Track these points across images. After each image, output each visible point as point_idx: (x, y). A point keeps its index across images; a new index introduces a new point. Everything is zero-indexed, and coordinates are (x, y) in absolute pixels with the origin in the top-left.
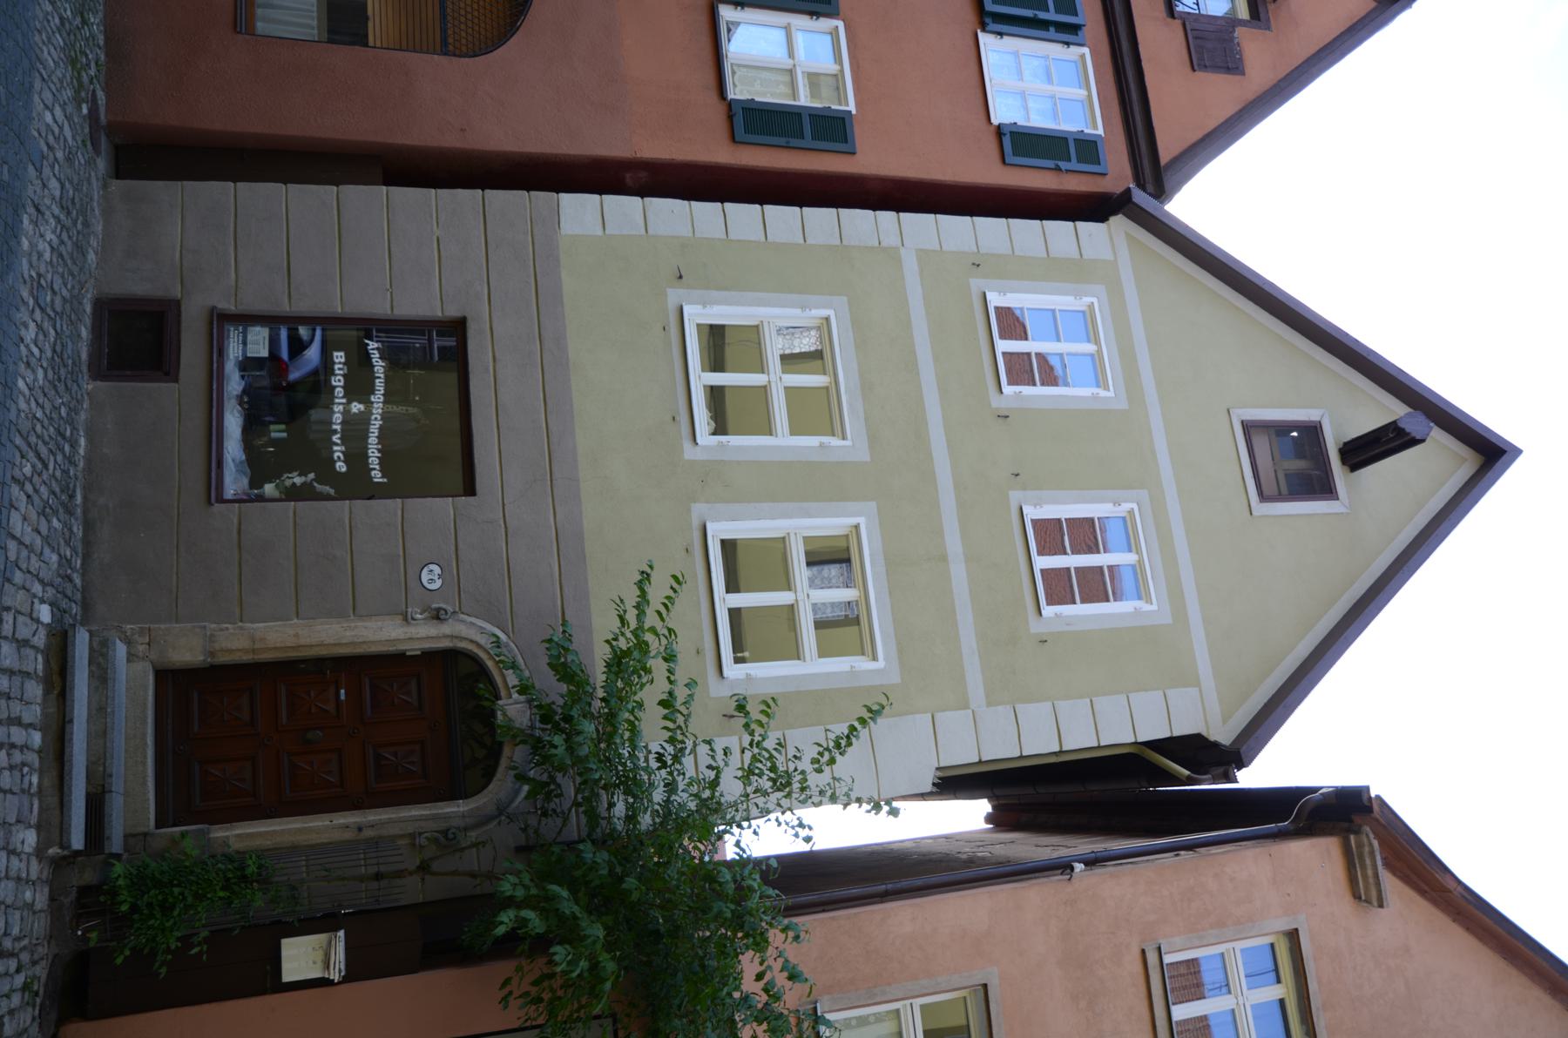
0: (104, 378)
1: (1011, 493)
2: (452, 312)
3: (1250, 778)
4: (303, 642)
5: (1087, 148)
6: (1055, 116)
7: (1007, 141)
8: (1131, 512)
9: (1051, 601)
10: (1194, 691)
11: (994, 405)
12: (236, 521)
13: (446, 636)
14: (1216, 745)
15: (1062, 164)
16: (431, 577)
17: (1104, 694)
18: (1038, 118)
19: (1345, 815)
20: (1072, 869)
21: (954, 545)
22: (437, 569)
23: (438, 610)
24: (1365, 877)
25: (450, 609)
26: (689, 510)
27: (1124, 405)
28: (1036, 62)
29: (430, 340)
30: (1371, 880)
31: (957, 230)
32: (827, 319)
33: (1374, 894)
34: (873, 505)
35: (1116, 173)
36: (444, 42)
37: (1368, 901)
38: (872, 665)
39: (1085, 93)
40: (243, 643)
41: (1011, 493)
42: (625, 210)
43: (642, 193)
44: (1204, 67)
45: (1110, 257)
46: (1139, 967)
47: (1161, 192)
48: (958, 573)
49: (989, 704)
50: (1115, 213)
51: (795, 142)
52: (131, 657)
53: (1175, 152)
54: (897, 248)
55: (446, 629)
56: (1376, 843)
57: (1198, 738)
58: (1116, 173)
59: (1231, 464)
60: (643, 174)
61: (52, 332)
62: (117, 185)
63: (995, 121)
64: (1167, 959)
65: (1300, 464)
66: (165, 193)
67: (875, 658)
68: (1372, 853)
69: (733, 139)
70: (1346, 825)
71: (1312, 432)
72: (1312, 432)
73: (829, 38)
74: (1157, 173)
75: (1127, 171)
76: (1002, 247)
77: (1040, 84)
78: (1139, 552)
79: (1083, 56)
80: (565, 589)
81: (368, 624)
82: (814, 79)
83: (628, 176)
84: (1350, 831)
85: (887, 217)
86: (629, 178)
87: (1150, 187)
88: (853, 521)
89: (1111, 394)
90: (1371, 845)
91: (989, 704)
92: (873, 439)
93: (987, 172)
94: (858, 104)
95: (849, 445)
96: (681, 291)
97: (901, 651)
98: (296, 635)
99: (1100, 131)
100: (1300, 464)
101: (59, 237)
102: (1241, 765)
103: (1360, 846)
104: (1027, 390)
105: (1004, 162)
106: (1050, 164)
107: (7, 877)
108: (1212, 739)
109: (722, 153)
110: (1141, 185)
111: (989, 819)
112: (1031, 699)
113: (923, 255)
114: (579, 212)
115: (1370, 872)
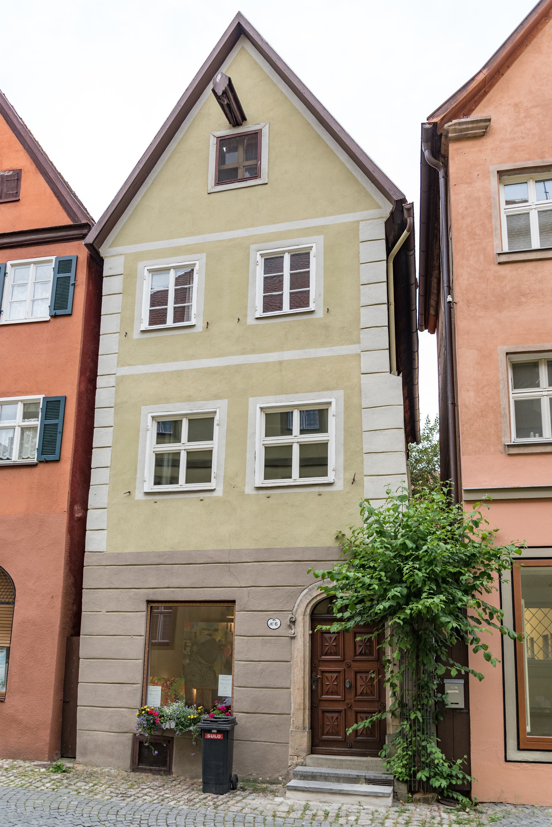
0: (170, 768)
1: (248, 324)
2: (143, 606)
3: (413, 193)
4: (302, 686)
5: (64, 266)
6: (46, 282)
7: (59, 312)
8: (262, 255)
9: (307, 305)
10: (362, 224)
11: (200, 329)
12: (242, 714)
13: (304, 619)
14: (392, 214)
15: (72, 282)
16: (275, 624)
17: (359, 278)
18: (46, 293)
19: (436, 141)
20: (450, 302)
21: (273, 357)
22: (271, 621)
23: (291, 622)
24: (472, 129)
25: (290, 616)
26: (248, 495)
27: (204, 255)
28: (15, 292)
29: (161, 613)
30: (475, 125)
31: (107, 344)
32: (153, 417)
33: (482, 124)
34: (251, 400)
35: (77, 251)
36: (8, 603)
37: (486, 128)
38: (333, 405)
39: (32, 265)
40: (300, 714)
41: (248, 324)
42: (94, 519)
43: (86, 509)
44: (17, 194)
45: (123, 257)
46: (508, 267)
47: (88, 226)
48: (288, 355)
49: (359, 342)
50: (98, 254)
51: (59, 429)
52: (303, 765)
53: (64, 214)
54: (116, 377)
55: (300, 618)
56: (454, 121)
57: (387, 223)
58: (77, 251)
59: (238, 195)
60: (76, 507)
61: (148, 790)
62: (79, 758)
63: (48, 318)
64: (506, 249)
65: (239, 158)
66: (82, 738)
67: (330, 403)
68: (460, 124)
69: (58, 461)
70: (443, 138)
71: (222, 141)
72: (222, 141)
73: (4, 406)
74: (77, 227)
75: (76, 243)
76: (116, 319)
77: (30, 286)
78: (284, 252)
79: (12, 265)
80: (284, 559)
81: (295, 655)
82: (26, 416)
83: (77, 515)
84: (446, 137)
85: (100, 382)
86: (78, 515)
87: (85, 231)
88: (258, 410)
89: (197, 262)
90: (455, 124)
91: (359, 342)
92: (217, 397)
93: (77, 322)
94: (40, 394)
95: (221, 411)
96: (137, 492)
97: (327, 389)
98: (298, 689)
99: (53, 258)
100: (239, 158)
101: (103, 784)
102: (404, 200)
103: (455, 131)
104: (194, 311)
105: (70, 315)
106: (71, 288)
107: (311, 823)
108: (388, 215)
109: (66, 465)
110: (83, 237)
111: (432, 332)
112: (358, 320)
113: (121, 364)
114: (95, 542)
115: (470, 126)
